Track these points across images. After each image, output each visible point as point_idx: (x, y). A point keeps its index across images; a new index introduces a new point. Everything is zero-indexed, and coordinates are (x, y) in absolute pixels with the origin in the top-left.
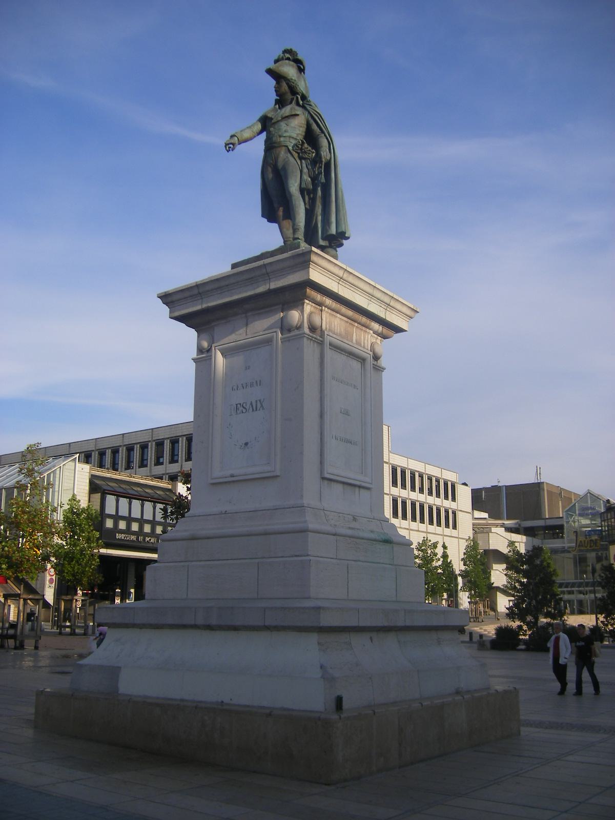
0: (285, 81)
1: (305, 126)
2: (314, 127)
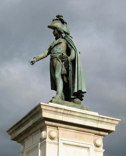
0: (56, 29)
1: (66, 46)
2: (69, 46)
